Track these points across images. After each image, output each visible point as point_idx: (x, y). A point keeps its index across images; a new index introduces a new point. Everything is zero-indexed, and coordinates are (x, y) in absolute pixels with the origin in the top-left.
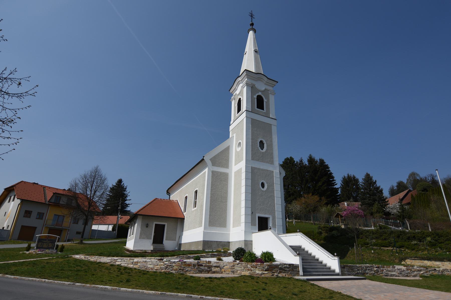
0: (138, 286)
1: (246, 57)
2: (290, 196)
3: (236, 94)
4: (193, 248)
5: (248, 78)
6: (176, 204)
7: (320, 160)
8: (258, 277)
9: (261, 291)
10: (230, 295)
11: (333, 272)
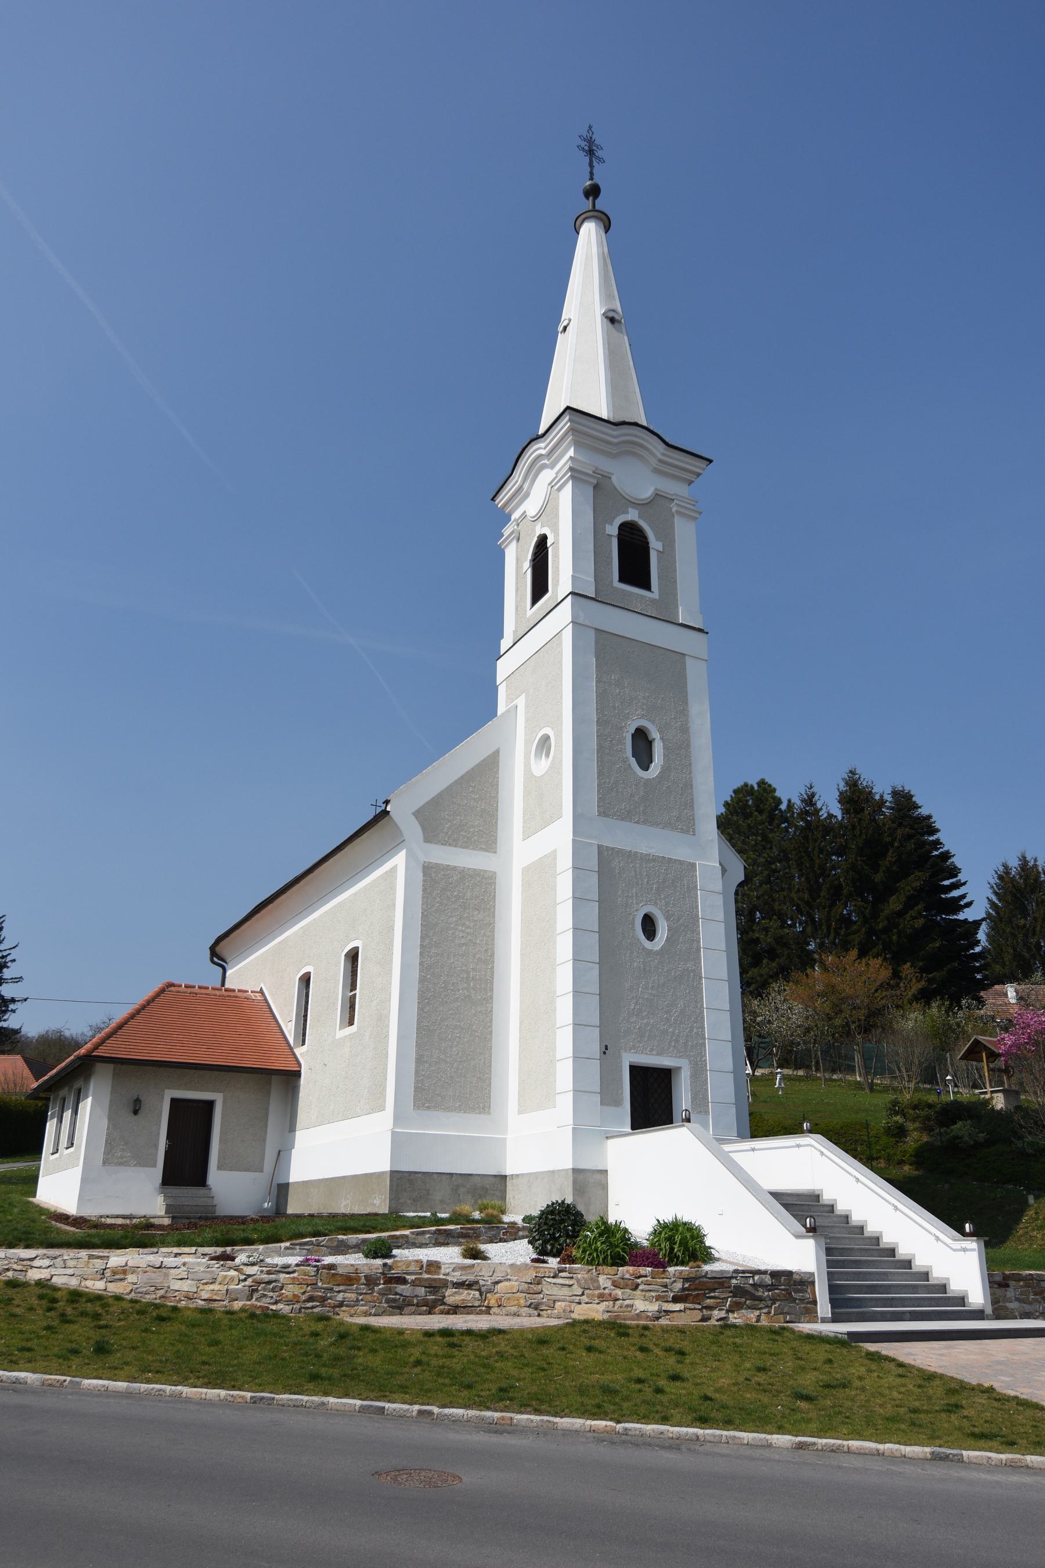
0: (147, 1371)
1: (565, 347)
2: (756, 962)
3: (524, 515)
4: (345, 1205)
5: (577, 444)
6: (251, 1010)
7: (895, 793)
8: (646, 1328)
9: (662, 1383)
10: (541, 1401)
11: (953, 1305)
